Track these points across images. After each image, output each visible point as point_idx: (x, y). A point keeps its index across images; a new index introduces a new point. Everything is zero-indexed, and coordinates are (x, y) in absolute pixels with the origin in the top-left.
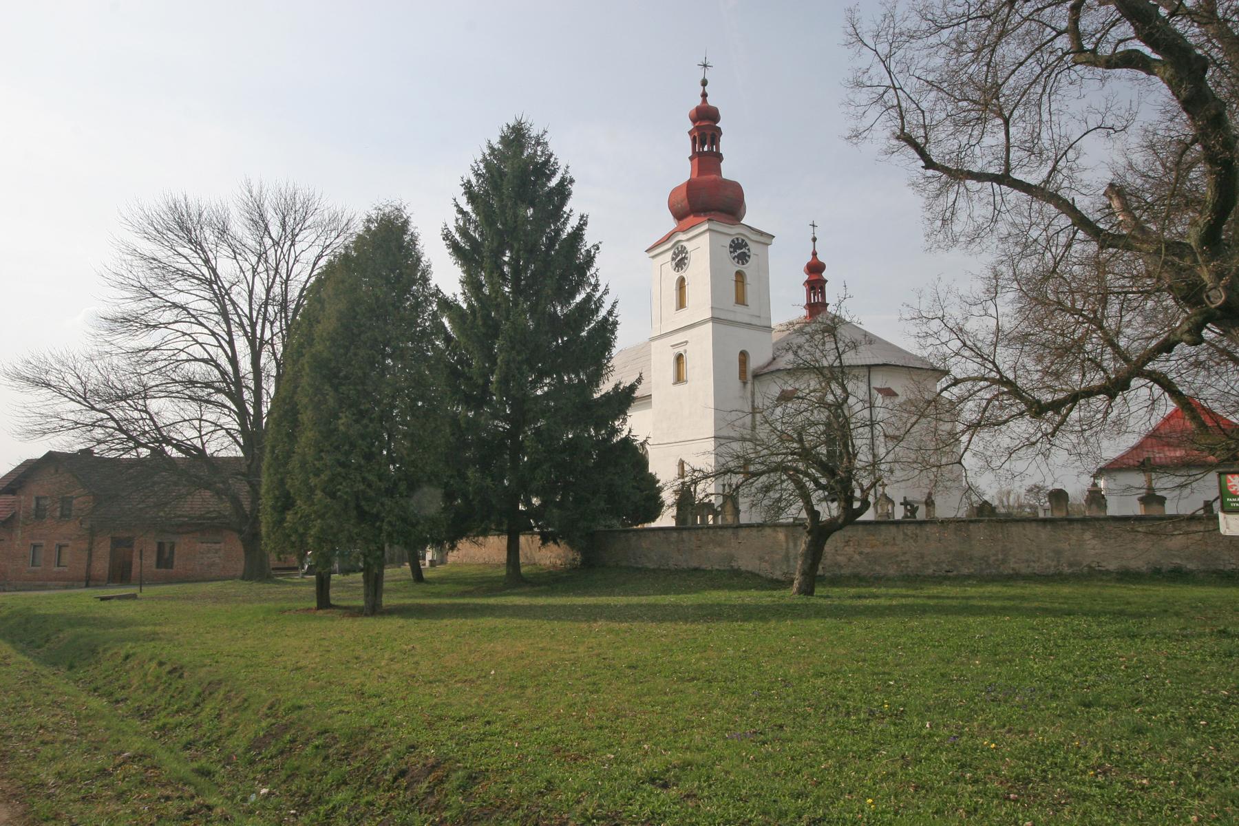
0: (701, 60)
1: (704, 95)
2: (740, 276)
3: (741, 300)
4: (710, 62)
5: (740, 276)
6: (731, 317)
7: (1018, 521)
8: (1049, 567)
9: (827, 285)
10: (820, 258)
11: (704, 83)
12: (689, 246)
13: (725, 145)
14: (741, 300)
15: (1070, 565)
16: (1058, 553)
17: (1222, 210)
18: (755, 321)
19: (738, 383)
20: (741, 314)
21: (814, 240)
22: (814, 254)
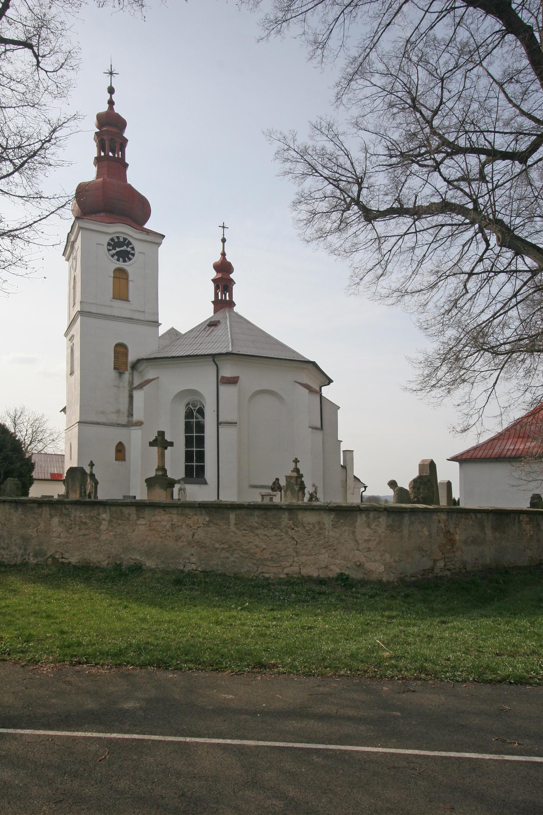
0: (107, 69)
1: (111, 103)
2: (121, 275)
3: (121, 293)
4: (115, 70)
5: (121, 275)
6: (107, 311)
7: (344, 510)
8: (16, 556)
9: (234, 287)
10: (228, 258)
11: (111, 91)
12: (135, 243)
13: (131, 154)
14: (121, 293)
15: (35, 556)
16: (26, 539)
17: (513, 25)
18: (136, 316)
19: (113, 374)
20: (120, 308)
21: (224, 240)
22: (223, 254)
